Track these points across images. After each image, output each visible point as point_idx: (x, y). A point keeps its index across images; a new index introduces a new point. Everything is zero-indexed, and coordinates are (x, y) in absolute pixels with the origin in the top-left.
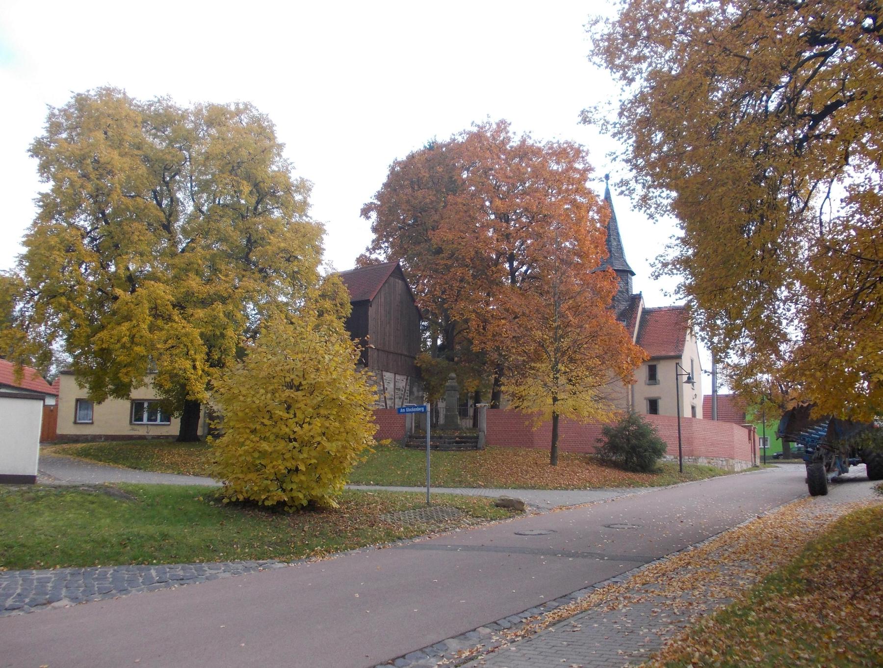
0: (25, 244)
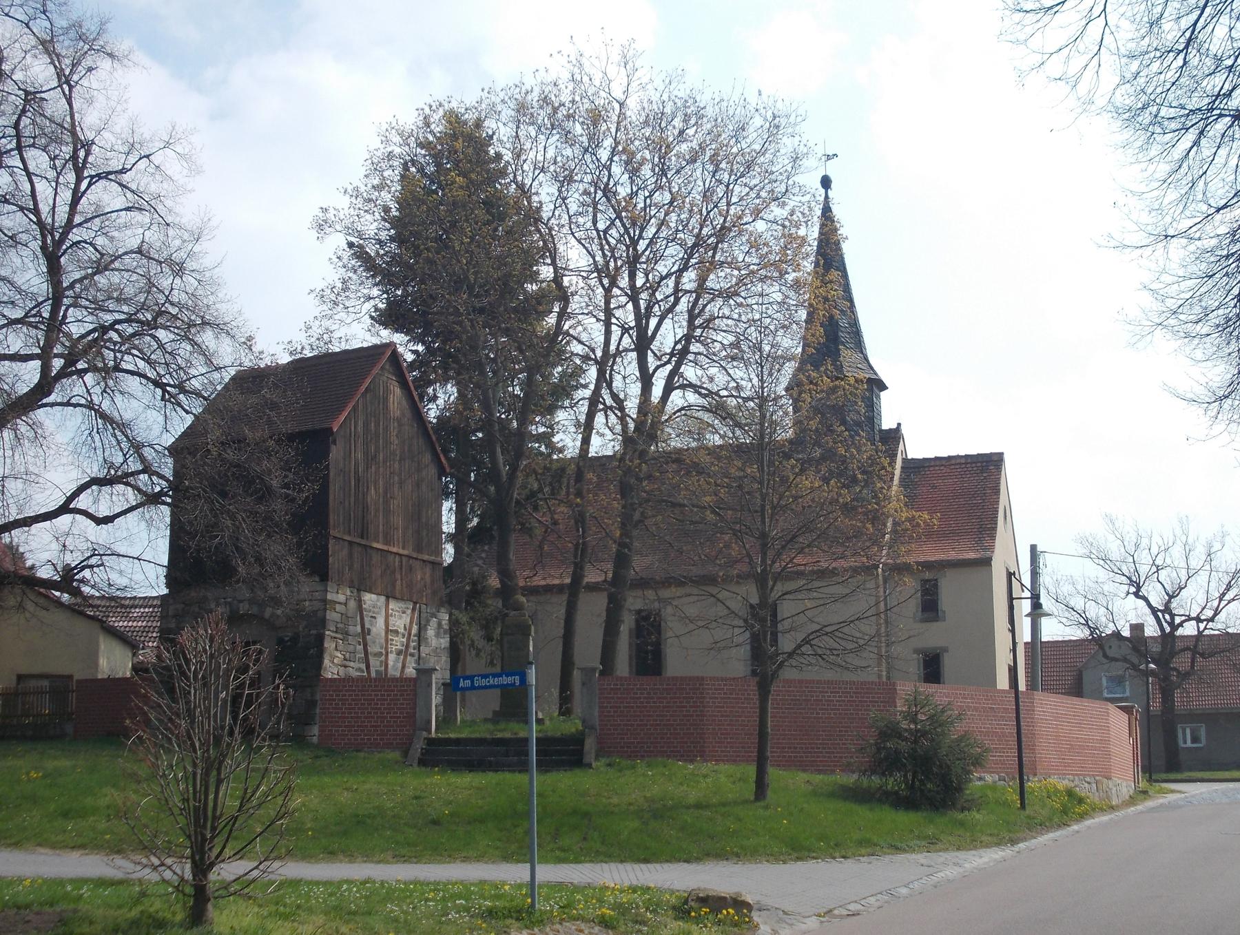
0: (452, 227)
